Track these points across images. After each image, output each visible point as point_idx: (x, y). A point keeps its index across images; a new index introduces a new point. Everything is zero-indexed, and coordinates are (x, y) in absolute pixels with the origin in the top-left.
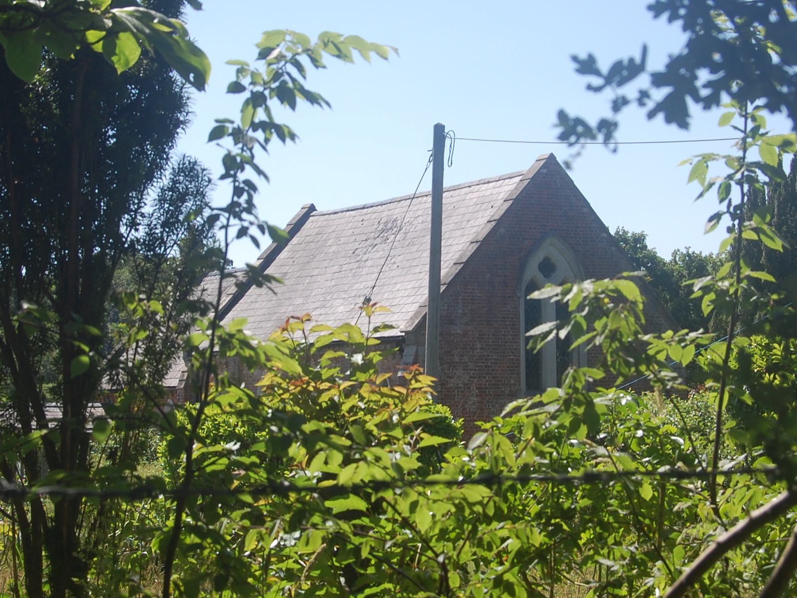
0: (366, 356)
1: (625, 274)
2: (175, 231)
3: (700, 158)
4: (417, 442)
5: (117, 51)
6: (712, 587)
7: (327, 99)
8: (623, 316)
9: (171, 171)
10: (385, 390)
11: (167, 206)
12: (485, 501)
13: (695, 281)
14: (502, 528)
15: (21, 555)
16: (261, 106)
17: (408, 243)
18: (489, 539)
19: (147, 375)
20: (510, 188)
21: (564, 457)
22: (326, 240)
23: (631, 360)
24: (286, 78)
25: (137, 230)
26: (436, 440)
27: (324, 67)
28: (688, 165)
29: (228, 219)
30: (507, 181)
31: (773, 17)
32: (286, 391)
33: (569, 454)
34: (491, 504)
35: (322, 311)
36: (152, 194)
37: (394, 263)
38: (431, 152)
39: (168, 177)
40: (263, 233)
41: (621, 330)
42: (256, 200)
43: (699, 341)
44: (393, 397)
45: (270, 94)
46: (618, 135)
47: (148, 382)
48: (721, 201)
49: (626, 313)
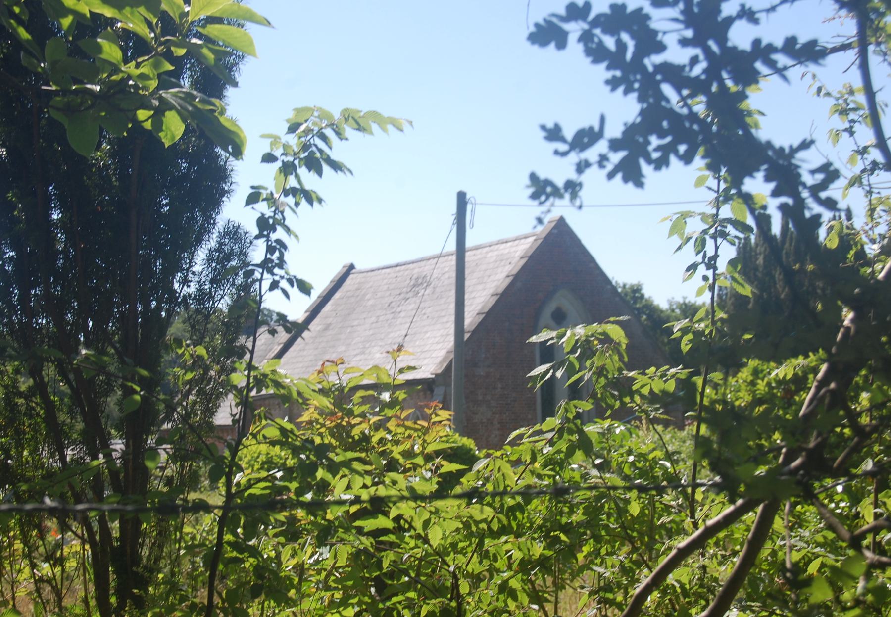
0: (393, 393)
1: (612, 319)
2: (222, 288)
3: (679, 215)
4: (437, 468)
5: (164, 128)
6: (692, 591)
7: (349, 167)
8: (608, 354)
9: (218, 234)
10: (409, 424)
11: (214, 265)
12: (489, 519)
13: (675, 323)
14: (506, 542)
15: (91, 571)
16: (292, 174)
17: (436, 296)
18: (495, 551)
19: (199, 413)
20: (525, 247)
21: (566, 481)
22: (365, 295)
23: (616, 393)
24: (314, 148)
25: (188, 286)
26: (454, 467)
27: (347, 139)
28: (668, 221)
29: (262, 274)
30: (523, 241)
31: (714, 88)
32: (323, 426)
33: (570, 478)
34: (496, 520)
35: (362, 357)
36: (201, 255)
37: (425, 314)
38: (454, 217)
39: (215, 240)
40: (292, 286)
41: (607, 367)
42: (287, 257)
43: (678, 376)
44: (416, 430)
45: (299, 162)
46: (584, 194)
47: (200, 419)
48: (697, 254)
49: (610, 352)
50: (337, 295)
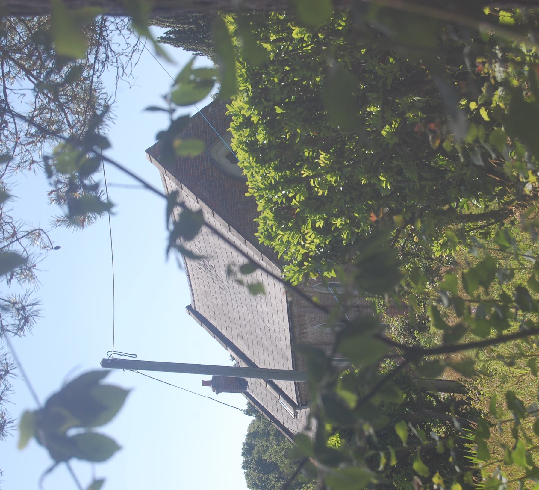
50: (213, 323)
